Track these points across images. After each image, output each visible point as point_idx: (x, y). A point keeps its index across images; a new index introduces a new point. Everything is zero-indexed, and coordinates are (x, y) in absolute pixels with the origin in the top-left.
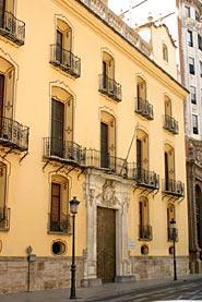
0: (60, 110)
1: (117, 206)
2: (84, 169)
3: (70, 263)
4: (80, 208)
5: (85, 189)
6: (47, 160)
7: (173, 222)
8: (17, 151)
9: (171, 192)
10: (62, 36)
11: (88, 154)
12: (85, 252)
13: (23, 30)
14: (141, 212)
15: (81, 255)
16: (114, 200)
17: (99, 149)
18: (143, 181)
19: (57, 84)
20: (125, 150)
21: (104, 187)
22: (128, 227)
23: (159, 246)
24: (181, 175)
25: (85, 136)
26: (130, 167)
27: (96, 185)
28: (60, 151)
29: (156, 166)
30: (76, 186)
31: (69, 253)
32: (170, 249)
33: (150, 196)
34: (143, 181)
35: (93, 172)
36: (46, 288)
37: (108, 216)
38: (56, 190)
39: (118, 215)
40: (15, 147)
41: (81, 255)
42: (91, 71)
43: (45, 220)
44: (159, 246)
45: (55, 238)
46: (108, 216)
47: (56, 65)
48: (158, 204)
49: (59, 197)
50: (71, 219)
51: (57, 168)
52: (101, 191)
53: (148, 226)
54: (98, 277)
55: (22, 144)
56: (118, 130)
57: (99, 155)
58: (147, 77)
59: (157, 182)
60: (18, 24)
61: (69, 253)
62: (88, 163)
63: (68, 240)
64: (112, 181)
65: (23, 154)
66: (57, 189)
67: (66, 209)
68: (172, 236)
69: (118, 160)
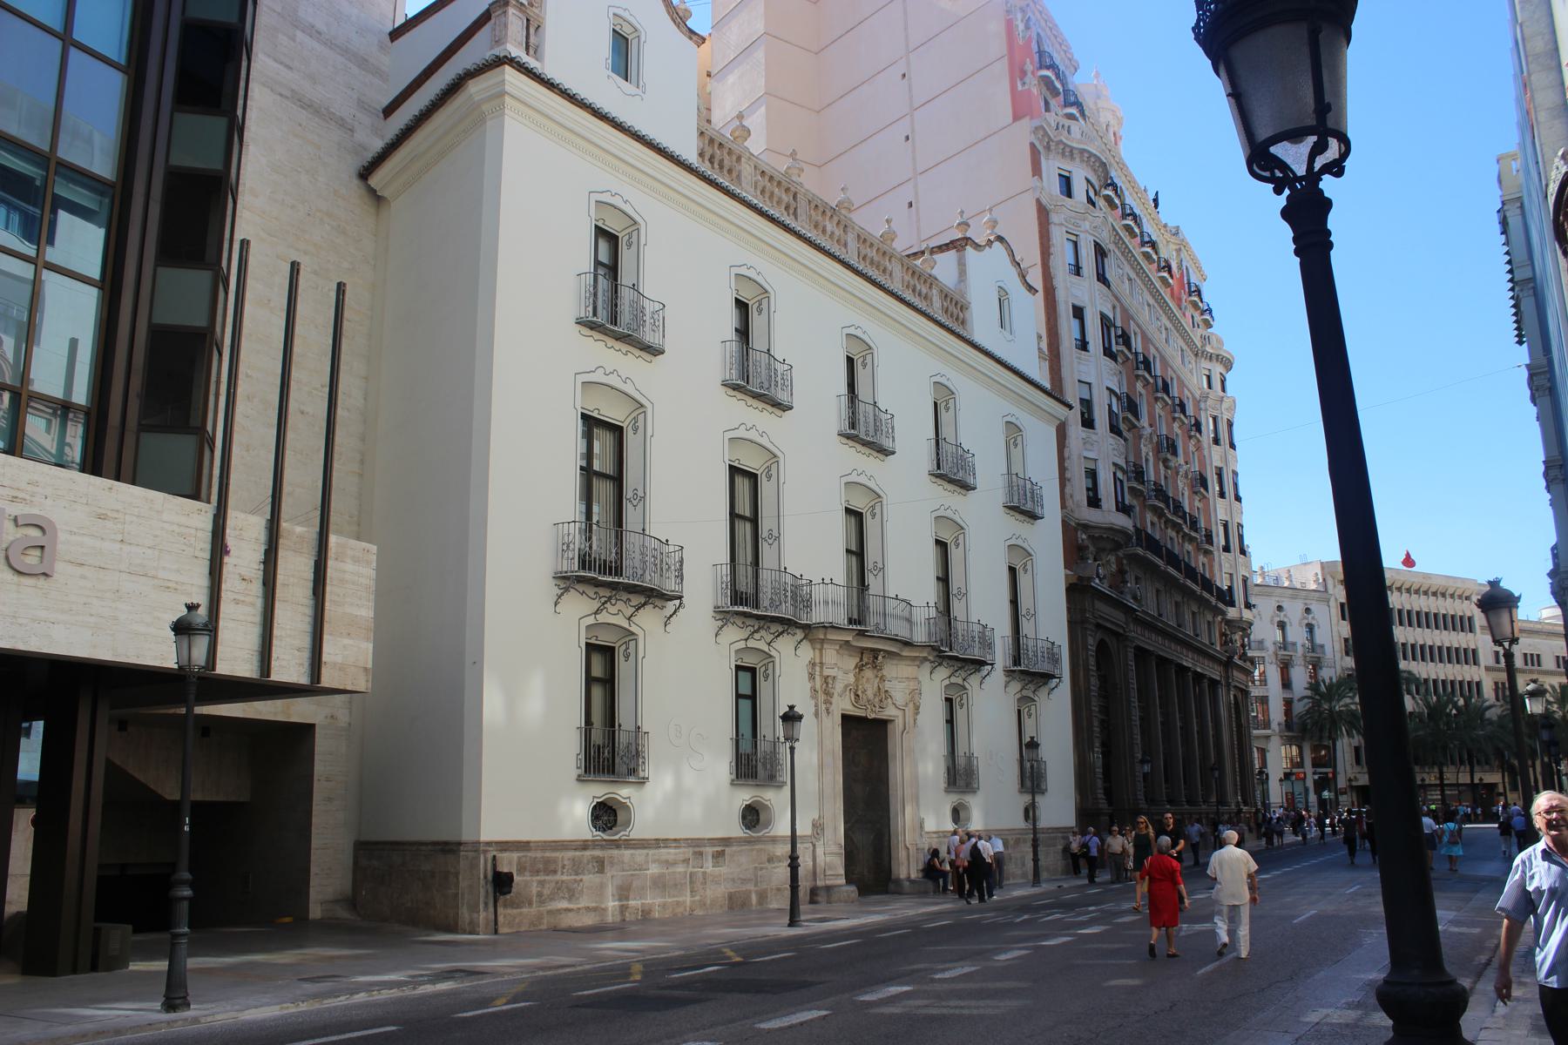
0: (607, 461)
1: (889, 712)
2: (807, 628)
3: (784, 850)
4: (806, 728)
5: (812, 676)
6: (723, 616)
7: (1033, 745)
8: (659, 603)
9: (1030, 677)
10: (611, 248)
11: (818, 593)
12: (818, 827)
13: (660, 326)
14: (950, 722)
15: (809, 832)
16: (883, 695)
17: (841, 578)
18: (953, 653)
19: (741, 433)
20: (907, 579)
21: (860, 668)
22: (918, 763)
23: (685, 789)
24: (1051, 623)
25: (808, 551)
26: (920, 615)
27: (842, 667)
28: (746, 602)
29: (984, 606)
30: (792, 673)
31: (782, 828)
32: (1026, 811)
33: (974, 680)
34: (953, 653)
35: (832, 636)
36: (731, 908)
37: (866, 742)
38: (745, 678)
39: (895, 732)
40: (653, 596)
41: (809, 832)
42: (696, 331)
43: (569, 748)
44: (685, 789)
45: (745, 796)
46: (866, 742)
47: (736, 388)
48: (991, 703)
49: (753, 697)
50: (784, 750)
51: (596, 605)
52: (852, 680)
53: (970, 758)
54: (849, 881)
55: (670, 586)
56: (889, 527)
57: (841, 594)
58: (874, 332)
59: (988, 645)
60: (649, 307)
61: (782, 828)
62: (818, 616)
63: (776, 799)
64: (875, 652)
65: (671, 606)
66: (749, 683)
67: (771, 727)
68: (1032, 779)
69: (891, 604)
